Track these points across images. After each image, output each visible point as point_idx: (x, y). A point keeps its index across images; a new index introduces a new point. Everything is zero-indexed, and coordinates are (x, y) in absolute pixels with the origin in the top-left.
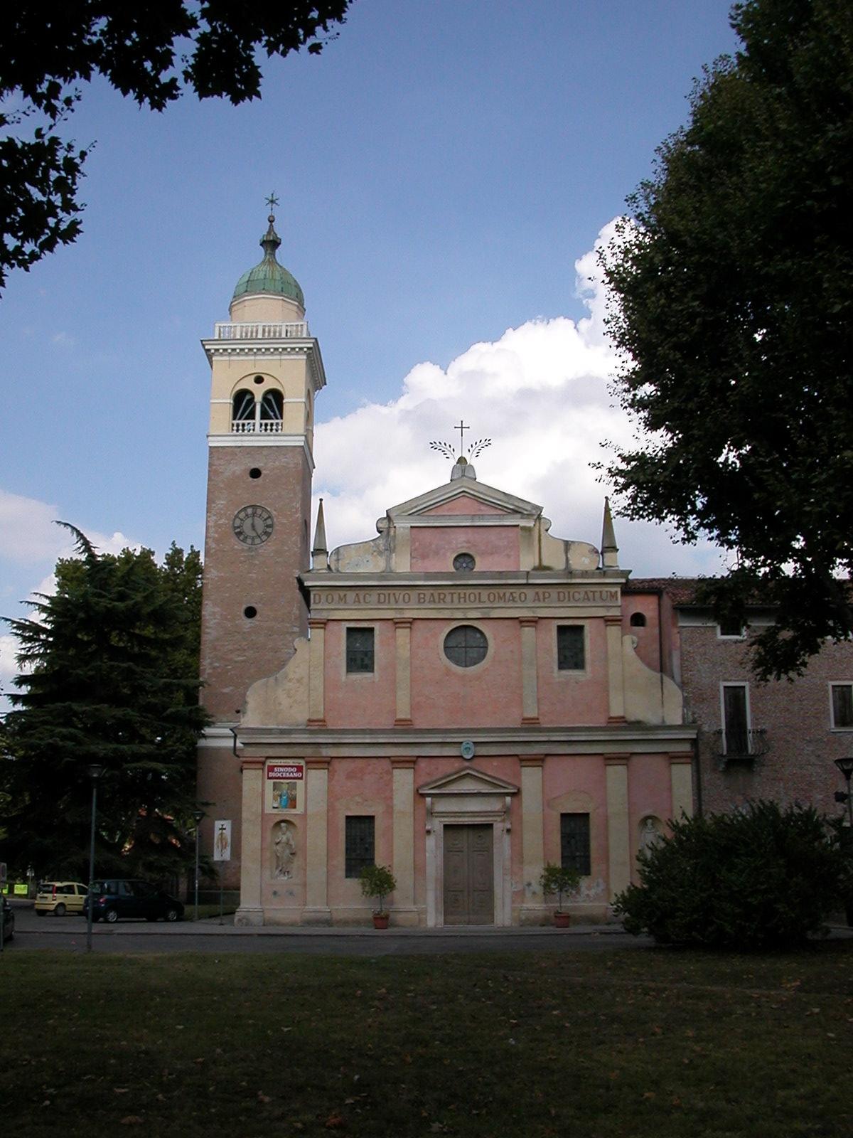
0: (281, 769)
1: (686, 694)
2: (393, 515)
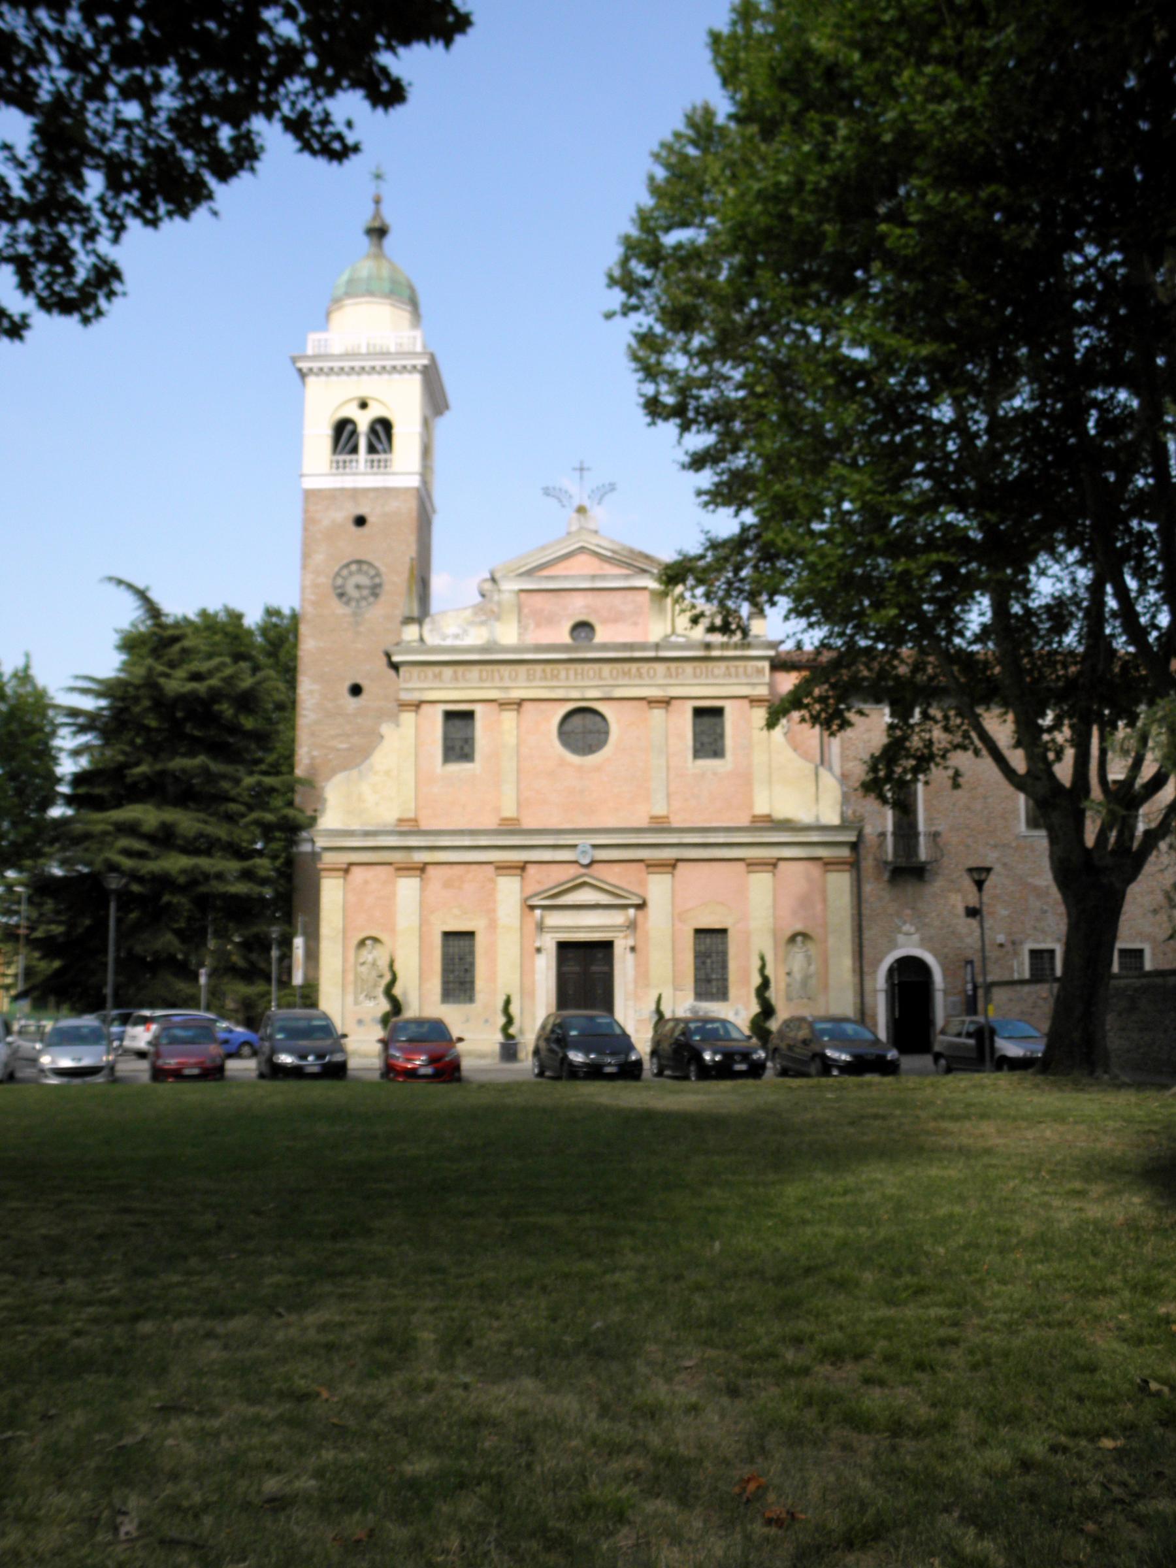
2: (498, 576)
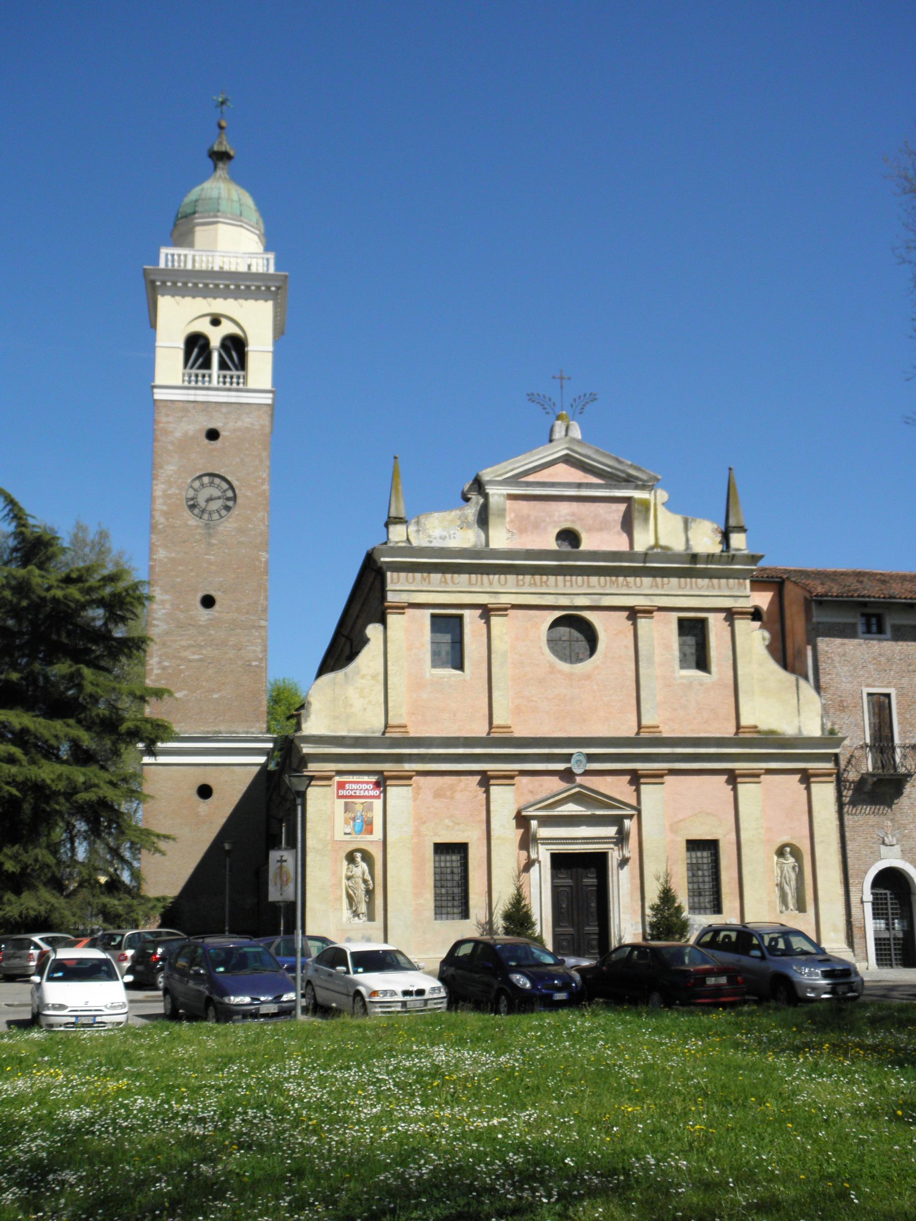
0: (354, 786)
1: (824, 702)
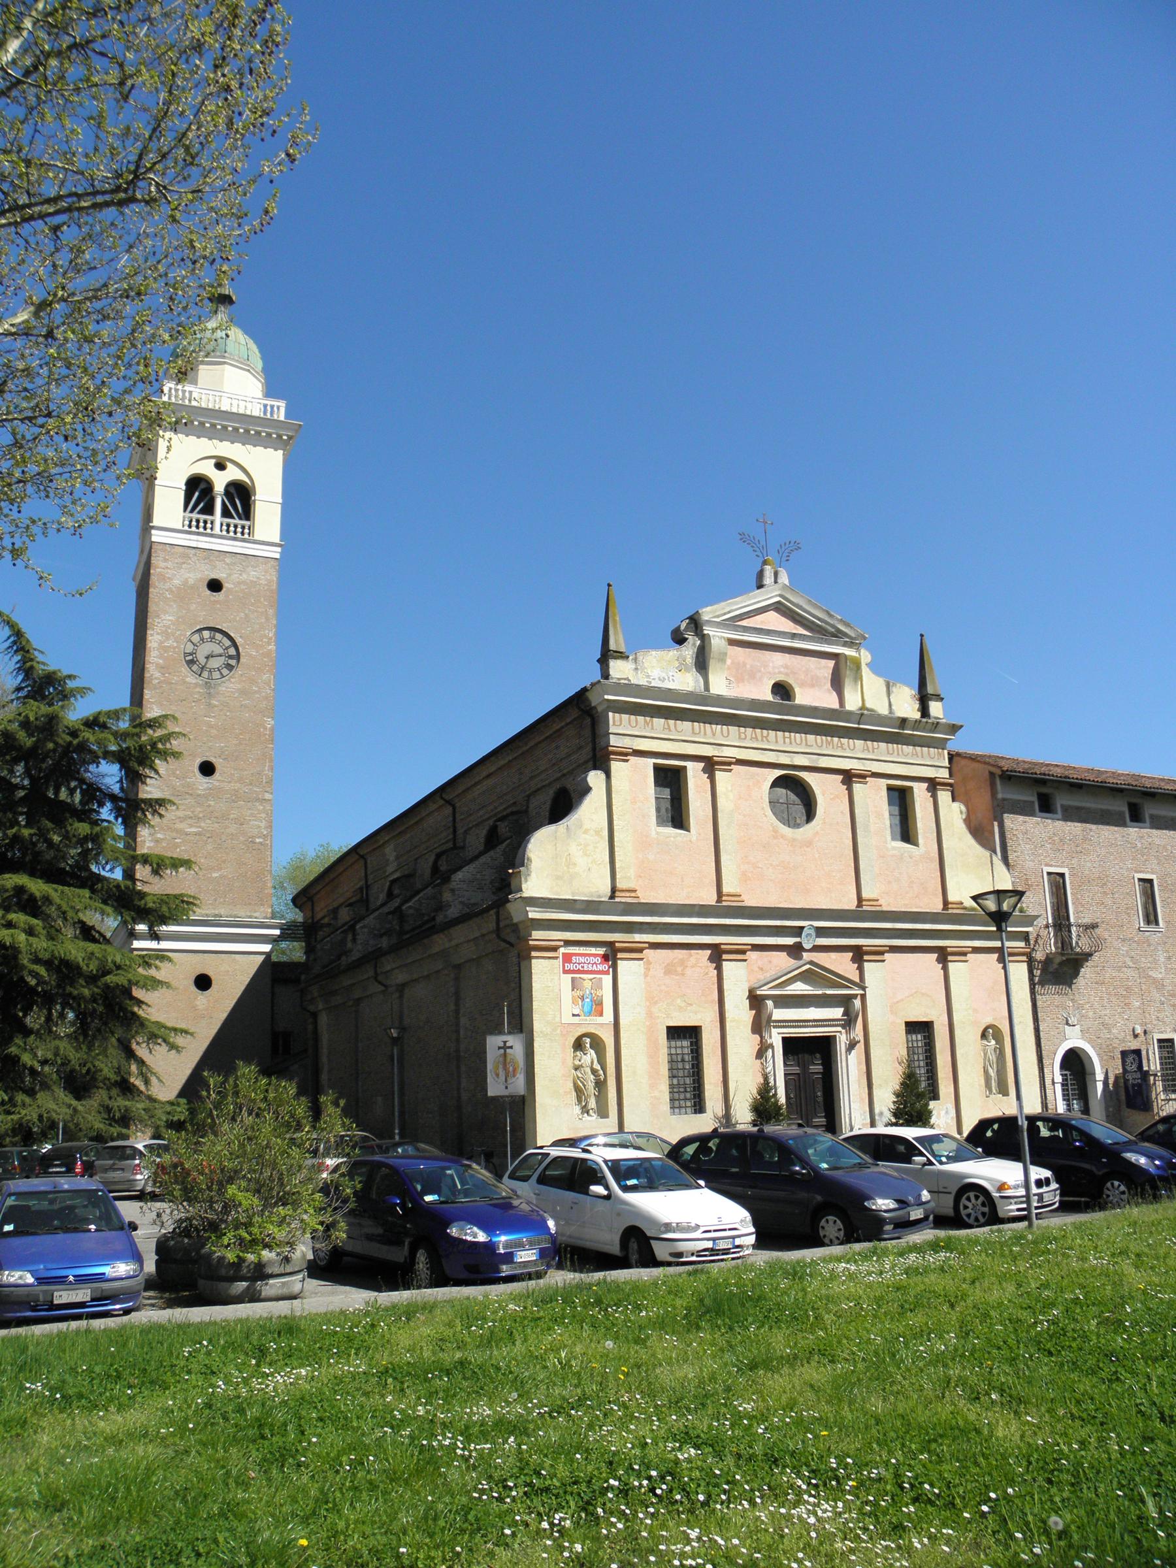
0: (582, 959)
